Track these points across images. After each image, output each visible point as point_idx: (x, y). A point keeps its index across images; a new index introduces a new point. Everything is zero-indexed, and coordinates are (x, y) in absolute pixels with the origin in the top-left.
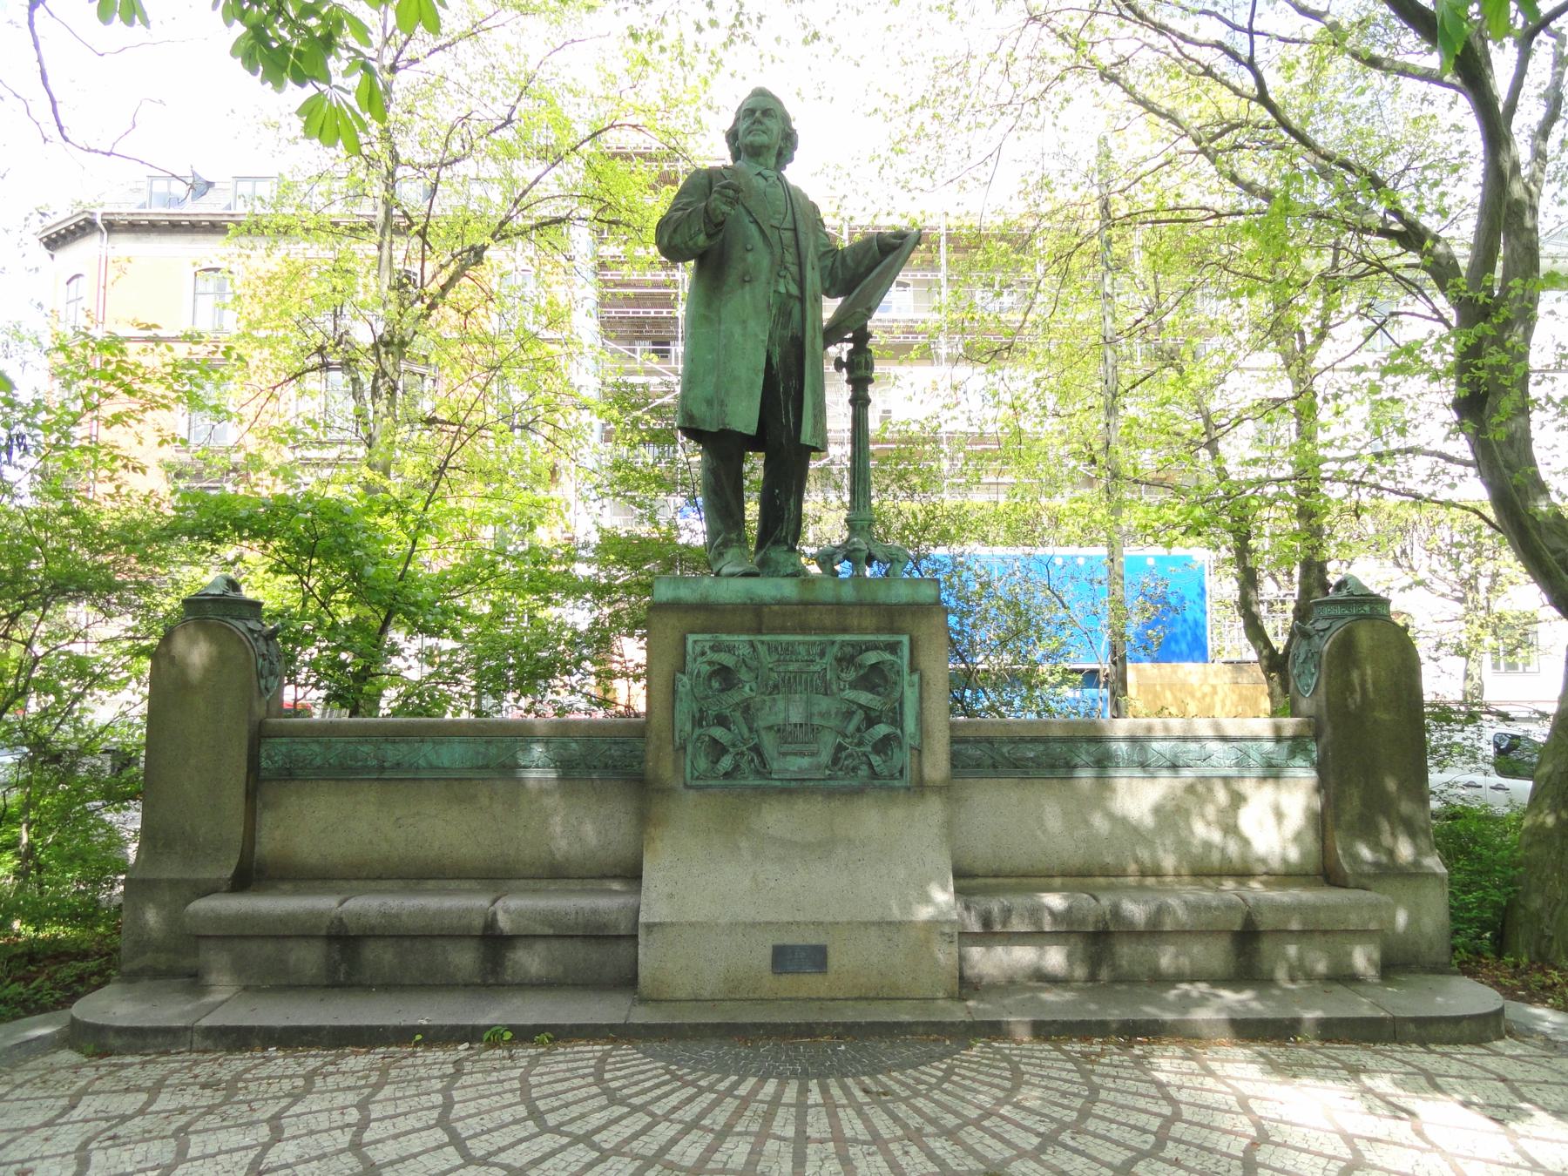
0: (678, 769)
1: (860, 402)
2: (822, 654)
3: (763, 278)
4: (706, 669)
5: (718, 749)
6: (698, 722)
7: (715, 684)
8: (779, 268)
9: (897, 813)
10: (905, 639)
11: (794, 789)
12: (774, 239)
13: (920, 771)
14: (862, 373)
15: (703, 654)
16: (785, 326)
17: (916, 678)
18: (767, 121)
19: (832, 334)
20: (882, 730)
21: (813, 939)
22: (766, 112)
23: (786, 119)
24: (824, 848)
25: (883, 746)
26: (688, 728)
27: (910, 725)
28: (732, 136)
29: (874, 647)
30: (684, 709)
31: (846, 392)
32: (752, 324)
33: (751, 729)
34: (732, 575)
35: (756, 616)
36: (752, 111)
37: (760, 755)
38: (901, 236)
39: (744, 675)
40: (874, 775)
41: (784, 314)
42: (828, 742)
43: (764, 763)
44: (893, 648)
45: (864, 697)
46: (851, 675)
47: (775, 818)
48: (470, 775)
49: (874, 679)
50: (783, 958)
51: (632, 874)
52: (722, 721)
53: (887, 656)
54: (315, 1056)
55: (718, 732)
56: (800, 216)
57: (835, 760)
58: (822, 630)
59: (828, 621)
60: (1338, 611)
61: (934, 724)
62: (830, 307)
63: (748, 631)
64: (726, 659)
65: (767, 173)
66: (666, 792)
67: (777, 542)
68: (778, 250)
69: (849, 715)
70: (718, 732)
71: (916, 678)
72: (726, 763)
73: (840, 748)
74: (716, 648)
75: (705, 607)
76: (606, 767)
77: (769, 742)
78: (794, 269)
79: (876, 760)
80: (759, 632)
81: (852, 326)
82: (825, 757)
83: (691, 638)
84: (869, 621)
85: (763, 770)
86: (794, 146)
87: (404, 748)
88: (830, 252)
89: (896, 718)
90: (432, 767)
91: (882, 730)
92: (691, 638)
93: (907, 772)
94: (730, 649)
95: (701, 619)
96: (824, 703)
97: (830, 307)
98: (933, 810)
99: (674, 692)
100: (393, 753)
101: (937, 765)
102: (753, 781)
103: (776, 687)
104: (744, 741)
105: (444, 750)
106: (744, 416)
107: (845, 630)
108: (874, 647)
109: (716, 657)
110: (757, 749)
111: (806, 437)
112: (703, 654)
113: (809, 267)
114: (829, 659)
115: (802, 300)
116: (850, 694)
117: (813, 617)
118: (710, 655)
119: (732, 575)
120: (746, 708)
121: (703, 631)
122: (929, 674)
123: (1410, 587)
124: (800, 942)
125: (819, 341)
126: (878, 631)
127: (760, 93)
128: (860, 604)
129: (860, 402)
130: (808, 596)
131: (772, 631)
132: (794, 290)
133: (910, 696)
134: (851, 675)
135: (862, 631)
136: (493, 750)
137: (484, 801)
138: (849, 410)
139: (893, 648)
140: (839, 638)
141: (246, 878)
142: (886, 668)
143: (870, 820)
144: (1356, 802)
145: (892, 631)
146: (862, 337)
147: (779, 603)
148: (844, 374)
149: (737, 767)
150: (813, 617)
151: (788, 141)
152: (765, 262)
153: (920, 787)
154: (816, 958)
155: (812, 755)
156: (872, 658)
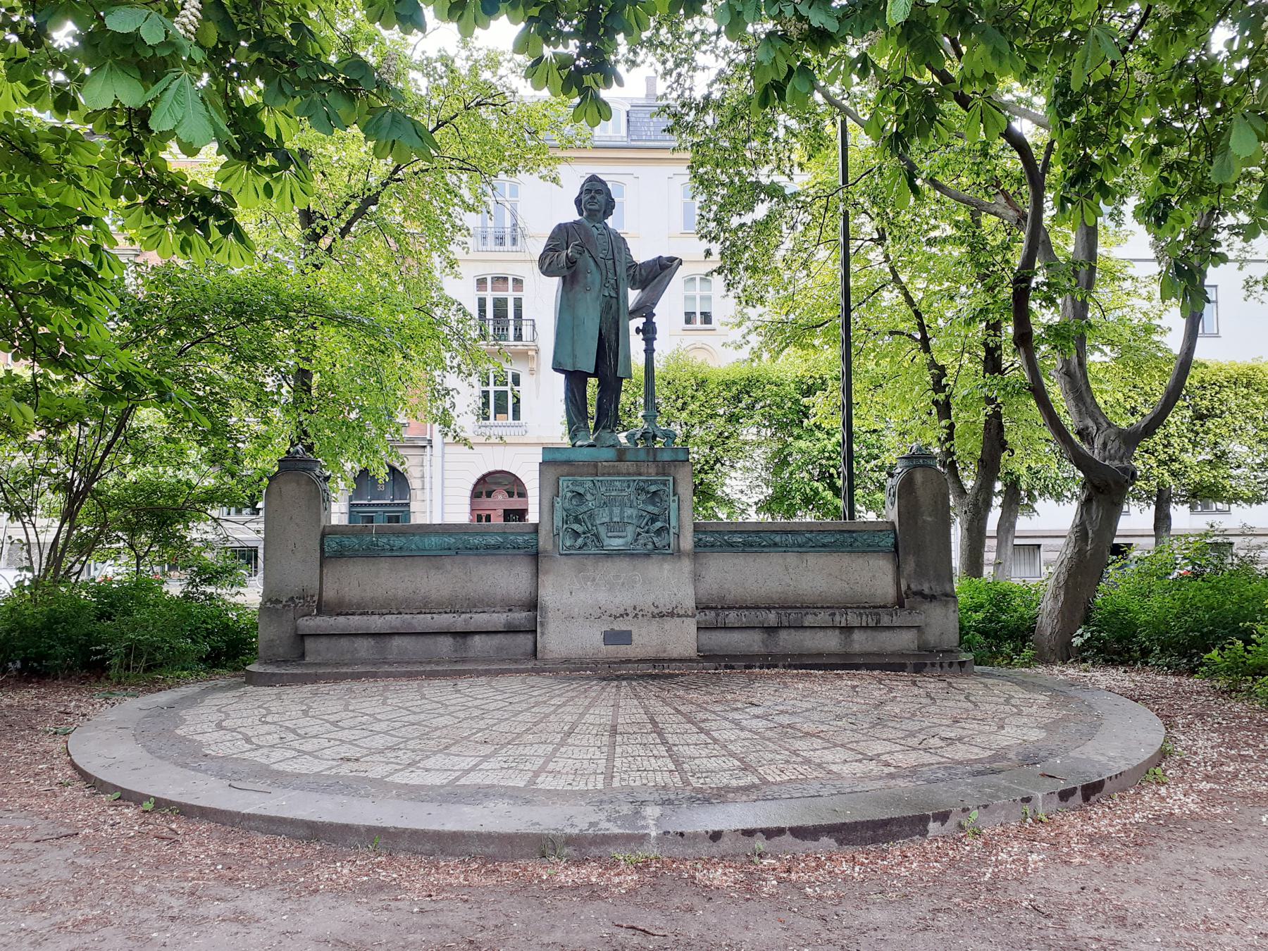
1: (649, 351)
4: (569, 494)
5: (576, 534)
6: (565, 522)
12: (602, 266)
14: (650, 336)
19: (634, 313)
20: (658, 524)
22: (598, 192)
27: (673, 522)
28: (578, 202)
29: (655, 482)
31: (643, 345)
35: (594, 468)
36: (589, 191)
38: (672, 259)
39: (589, 497)
40: (656, 548)
44: (665, 483)
45: (650, 508)
48: (440, 553)
53: (662, 487)
54: (340, 892)
55: (576, 527)
56: (617, 243)
58: (629, 474)
61: (686, 517)
63: (591, 475)
70: (576, 527)
72: (580, 541)
81: (645, 309)
82: (629, 539)
86: (613, 207)
88: (632, 265)
90: (419, 549)
91: (658, 524)
94: (582, 484)
95: (566, 469)
96: (628, 512)
97: (633, 296)
98: (686, 565)
101: (687, 542)
102: (594, 551)
107: (640, 474)
108: (655, 482)
110: (597, 536)
114: (632, 489)
115: (617, 298)
121: (568, 475)
123: (938, 386)
126: (657, 474)
129: (649, 351)
131: (603, 475)
132: (614, 295)
133: (674, 506)
135: (649, 474)
137: (449, 567)
138: (644, 355)
144: (913, 565)
145: (664, 475)
146: (650, 316)
149: (585, 544)
153: (678, 554)
156: (653, 488)
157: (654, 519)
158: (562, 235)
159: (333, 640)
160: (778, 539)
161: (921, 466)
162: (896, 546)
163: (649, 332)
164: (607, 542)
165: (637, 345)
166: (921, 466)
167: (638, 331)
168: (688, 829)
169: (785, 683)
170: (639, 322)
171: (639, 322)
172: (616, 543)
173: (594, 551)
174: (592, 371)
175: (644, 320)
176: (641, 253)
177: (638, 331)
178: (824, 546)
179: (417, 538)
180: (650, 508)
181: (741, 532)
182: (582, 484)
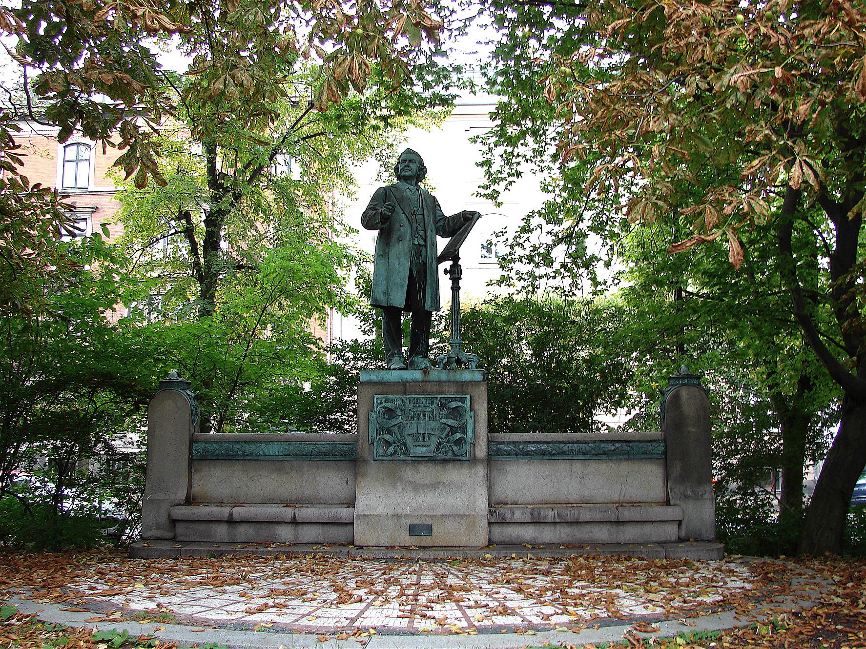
0: (371, 453)
1: (456, 289)
2: (432, 403)
3: (408, 238)
5: (388, 444)
6: (379, 433)
7: (386, 417)
8: (414, 233)
9: (465, 471)
10: (468, 397)
11: (417, 461)
13: (475, 454)
14: (456, 276)
15: (381, 403)
16: (418, 258)
17: (472, 413)
18: (411, 165)
20: (458, 435)
21: (428, 521)
23: (421, 162)
24: (433, 486)
25: (459, 442)
26: (375, 435)
29: (455, 400)
30: (373, 426)
32: (402, 259)
33: (401, 436)
34: (394, 369)
37: (406, 446)
38: (473, 213)
39: (399, 412)
41: (418, 253)
42: (434, 441)
43: (407, 450)
44: (463, 400)
45: (450, 422)
46: (445, 412)
47: (409, 473)
49: (456, 413)
50: (413, 530)
51: (351, 504)
52: (389, 432)
53: (460, 404)
55: (387, 437)
57: (438, 449)
58: (433, 393)
59: (435, 389)
60: (674, 382)
62: (442, 243)
63: (401, 393)
64: (389, 405)
65: (411, 188)
66: (365, 461)
67: (417, 354)
68: (415, 225)
69: (443, 429)
70: (387, 437)
71: (472, 413)
73: (440, 444)
74: (387, 400)
75: (381, 383)
76: (341, 455)
77: (409, 441)
78: (422, 233)
79: (455, 448)
80: (405, 394)
81: (452, 254)
82: (433, 448)
83: (376, 397)
84: (452, 389)
85: (407, 452)
87: (253, 446)
89: (464, 431)
91: (458, 435)
92: (376, 397)
93: (469, 454)
94: (392, 401)
95: (380, 388)
96: (433, 424)
97: (442, 243)
98: (481, 471)
99: (369, 420)
100: (249, 449)
101: (481, 451)
102: (402, 457)
103: (412, 417)
104: (399, 441)
105: (270, 447)
106: (399, 299)
107: (442, 393)
108: (455, 400)
109: (386, 405)
110: (405, 444)
111: (428, 306)
112: (381, 403)
113: (429, 231)
115: (426, 246)
116: (444, 420)
117: (429, 387)
118: (384, 404)
119: (394, 369)
120: (400, 426)
122: (479, 412)
124: (421, 523)
125: (434, 263)
126: (457, 393)
127: (409, 151)
128: (449, 381)
129: (456, 289)
130: (426, 378)
131: (411, 393)
133: (470, 422)
134: (445, 412)
135: (450, 393)
136: (291, 448)
139: (463, 400)
140: (439, 396)
141: (190, 500)
142: (460, 409)
143: (454, 474)
144: (678, 468)
146: (456, 259)
147: (414, 381)
148: (448, 275)
149: (396, 452)
150: (429, 387)
151: (422, 171)
152: (409, 231)
153: (474, 461)
154: (429, 529)
155: (428, 446)
156: (454, 405)
157: (453, 430)
158: (382, 197)
159: (264, 526)
160: (565, 448)
161: (685, 385)
162: (665, 452)
163: (455, 274)
164: (413, 450)
165: (445, 283)
166: (685, 385)
167: (446, 272)
168: (42, 617)
169: (591, 570)
170: (447, 264)
171: (447, 264)
172: (420, 451)
173: (402, 457)
174: (403, 306)
175: (451, 263)
176: (449, 209)
177: (446, 272)
178: (605, 454)
179: (264, 445)
180: (450, 422)
181: (534, 442)
182: (392, 401)
